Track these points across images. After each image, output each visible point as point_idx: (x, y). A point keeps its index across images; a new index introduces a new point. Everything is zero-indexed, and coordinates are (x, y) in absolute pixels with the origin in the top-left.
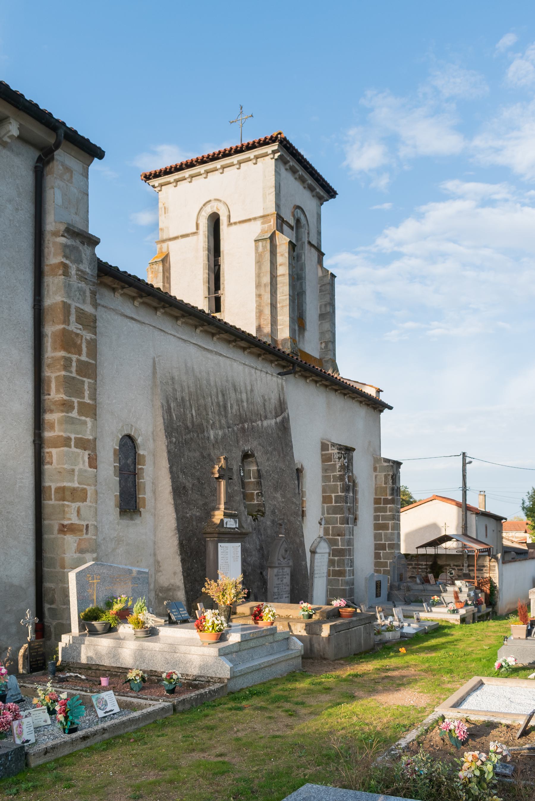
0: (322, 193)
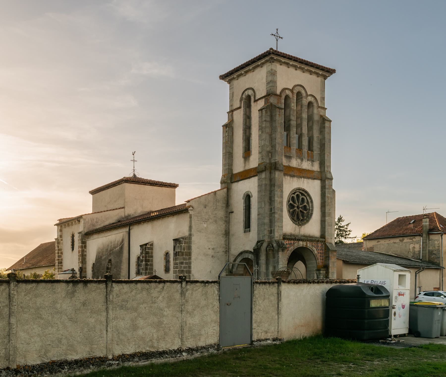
0: (264, 61)
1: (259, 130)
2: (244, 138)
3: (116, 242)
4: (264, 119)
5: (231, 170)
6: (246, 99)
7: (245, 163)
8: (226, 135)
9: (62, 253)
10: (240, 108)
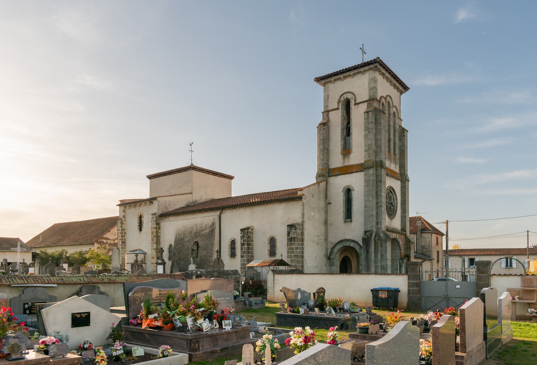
1: (365, 130)
2: (343, 136)
3: (204, 225)
4: (370, 121)
5: (328, 165)
6: (343, 102)
7: (344, 160)
8: (324, 132)
9: (125, 233)
10: (338, 109)
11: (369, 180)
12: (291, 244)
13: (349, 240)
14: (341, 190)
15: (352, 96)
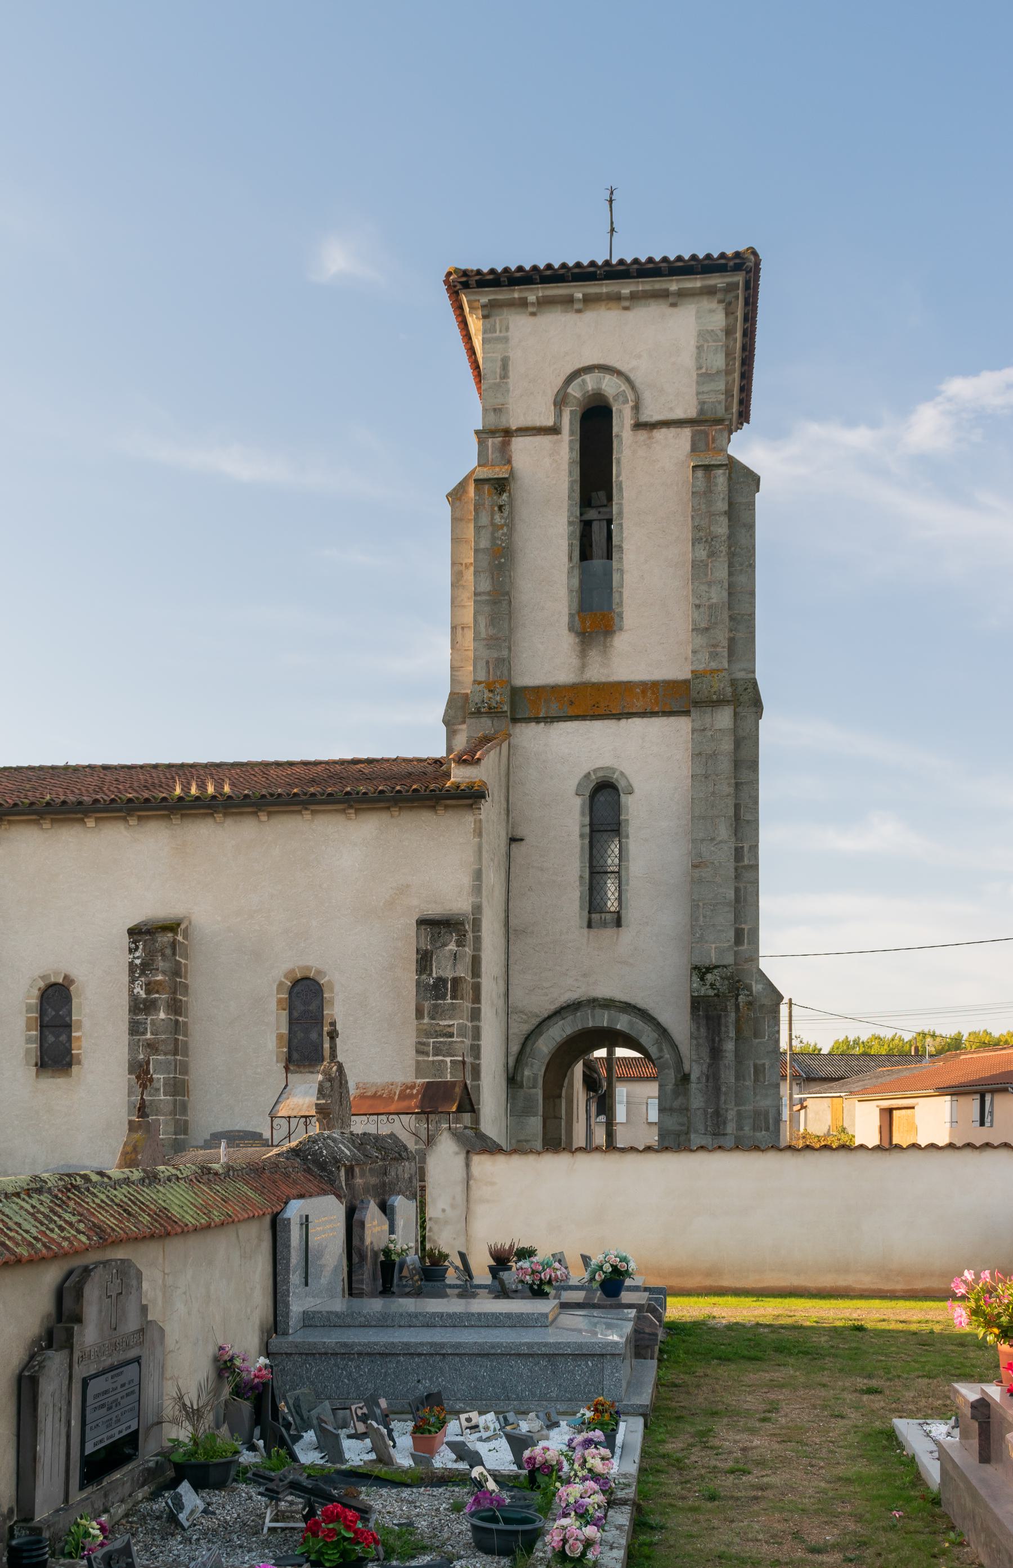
0: (698, 284)
1: (695, 541)
7: (583, 654)
10: (554, 430)
11: (714, 755)
12: (436, 1013)
13: (608, 1004)
14: (573, 783)
15: (624, 387)
